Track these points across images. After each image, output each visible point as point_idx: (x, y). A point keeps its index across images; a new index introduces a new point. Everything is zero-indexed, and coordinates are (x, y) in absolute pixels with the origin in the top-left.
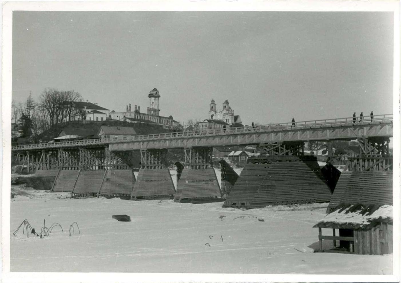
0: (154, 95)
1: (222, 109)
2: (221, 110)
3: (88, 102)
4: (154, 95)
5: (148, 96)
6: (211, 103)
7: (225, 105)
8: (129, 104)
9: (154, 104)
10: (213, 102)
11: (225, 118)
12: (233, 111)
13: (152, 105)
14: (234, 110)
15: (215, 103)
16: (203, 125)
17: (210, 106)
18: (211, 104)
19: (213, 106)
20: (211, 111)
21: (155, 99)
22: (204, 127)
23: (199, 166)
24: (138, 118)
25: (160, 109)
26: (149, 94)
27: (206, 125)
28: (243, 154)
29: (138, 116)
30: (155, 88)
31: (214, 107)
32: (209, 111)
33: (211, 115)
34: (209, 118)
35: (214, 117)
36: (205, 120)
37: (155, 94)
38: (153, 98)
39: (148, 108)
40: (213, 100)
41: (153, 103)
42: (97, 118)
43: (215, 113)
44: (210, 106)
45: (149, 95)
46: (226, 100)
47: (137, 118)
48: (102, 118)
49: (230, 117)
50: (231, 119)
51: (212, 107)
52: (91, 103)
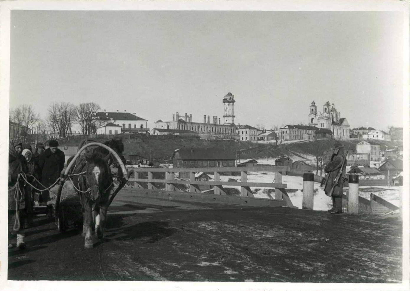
0: (229, 100)
1: (322, 112)
2: (322, 113)
3: (125, 113)
4: (229, 100)
5: (222, 101)
6: (311, 105)
7: (326, 107)
8: (177, 113)
9: (228, 110)
10: (314, 104)
11: (320, 122)
12: (339, 113)
13: (226, 111)
14: (340, 112)
15: (316, 105)
16: (283, 132)
17: (310, 109)
18: (311, 106)
19: (313, 109)
20: (311, 114)
21: (229, 104)
22: (284, 133)
23: (22, 203)
24: (185, 129)
25: (235, 115)
26: (224, 99)
27: (287, 131)
28: (204, 176)
29: (182, 126)
30: (229, 93)
31: (314, 110)
32: (309, 114)
33: (311, 118)
34: (155, 127)
35: (314, 120)
36: (286, 126)
37: (229, 99)
38: (227, 104)
39: (204, 115)
40: (313, 102)
41: (227, 108)
42: (110, 132)
43: (315, 116)
44: (310, 108)
45: (224, 99)
46: (328, 101)
47: (181, 129)
48: (116, 132)
49: (325, 121)
50: (326, 123)
51: (312, 110)
52: (129, 113)
